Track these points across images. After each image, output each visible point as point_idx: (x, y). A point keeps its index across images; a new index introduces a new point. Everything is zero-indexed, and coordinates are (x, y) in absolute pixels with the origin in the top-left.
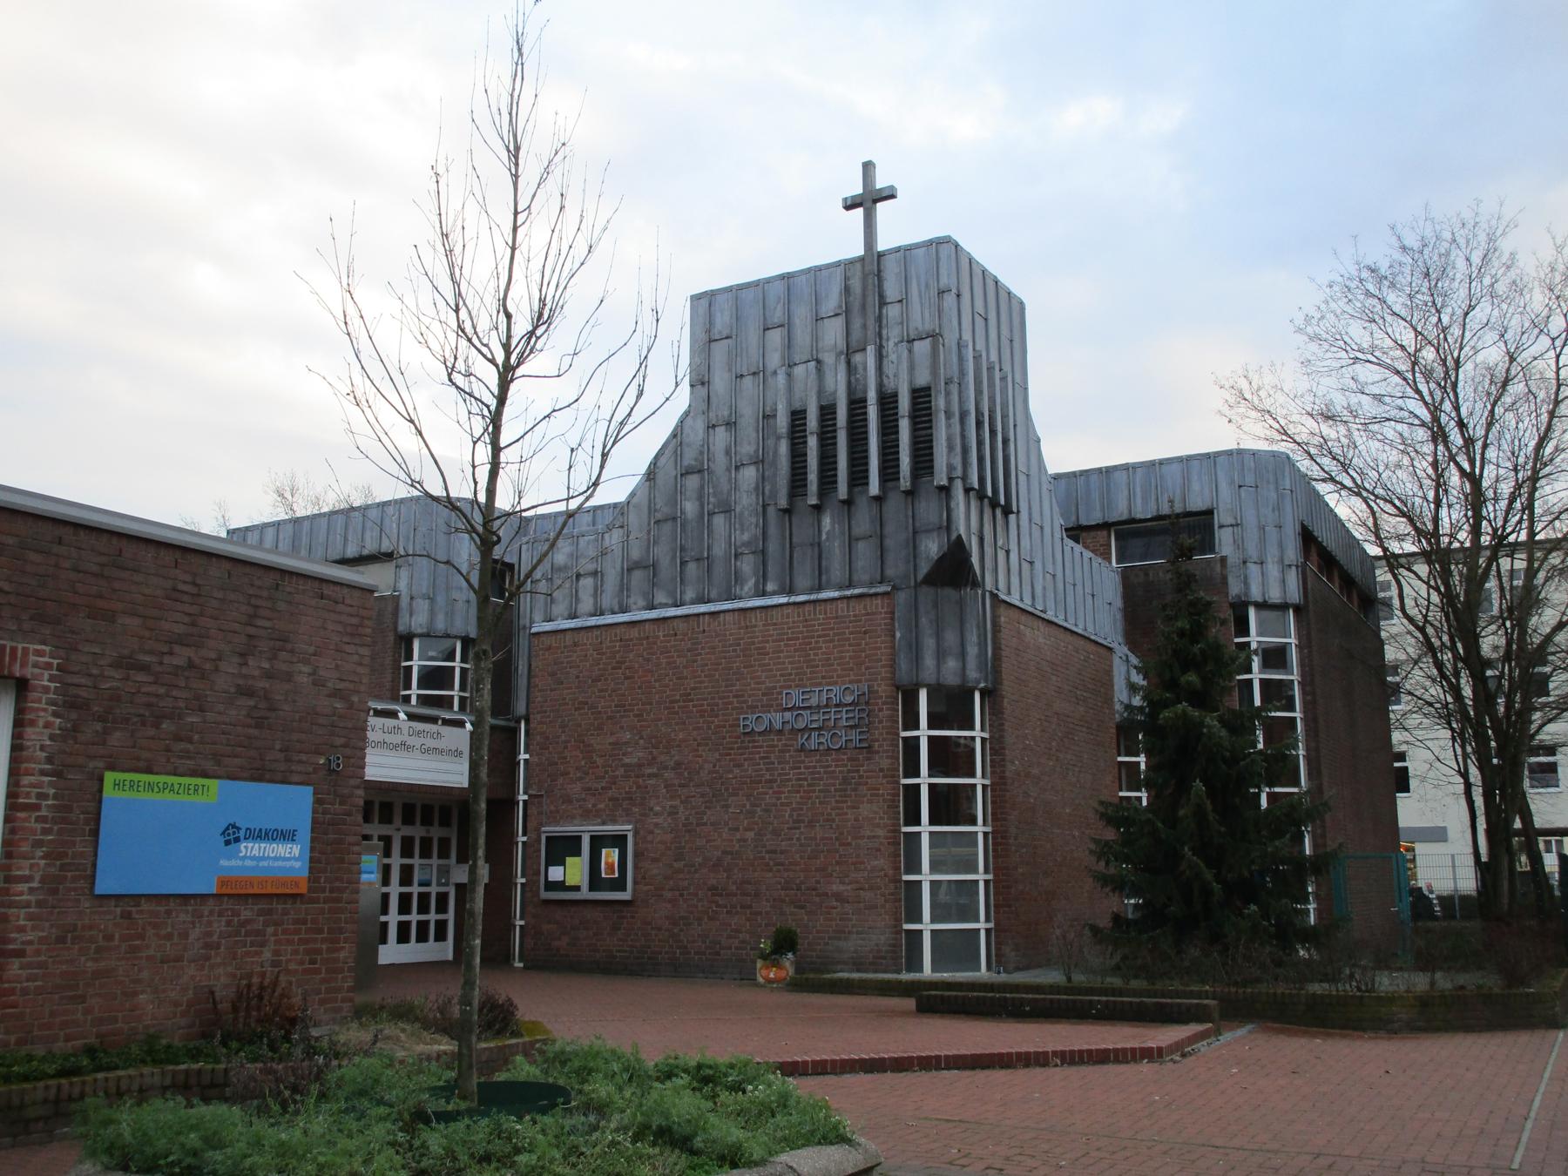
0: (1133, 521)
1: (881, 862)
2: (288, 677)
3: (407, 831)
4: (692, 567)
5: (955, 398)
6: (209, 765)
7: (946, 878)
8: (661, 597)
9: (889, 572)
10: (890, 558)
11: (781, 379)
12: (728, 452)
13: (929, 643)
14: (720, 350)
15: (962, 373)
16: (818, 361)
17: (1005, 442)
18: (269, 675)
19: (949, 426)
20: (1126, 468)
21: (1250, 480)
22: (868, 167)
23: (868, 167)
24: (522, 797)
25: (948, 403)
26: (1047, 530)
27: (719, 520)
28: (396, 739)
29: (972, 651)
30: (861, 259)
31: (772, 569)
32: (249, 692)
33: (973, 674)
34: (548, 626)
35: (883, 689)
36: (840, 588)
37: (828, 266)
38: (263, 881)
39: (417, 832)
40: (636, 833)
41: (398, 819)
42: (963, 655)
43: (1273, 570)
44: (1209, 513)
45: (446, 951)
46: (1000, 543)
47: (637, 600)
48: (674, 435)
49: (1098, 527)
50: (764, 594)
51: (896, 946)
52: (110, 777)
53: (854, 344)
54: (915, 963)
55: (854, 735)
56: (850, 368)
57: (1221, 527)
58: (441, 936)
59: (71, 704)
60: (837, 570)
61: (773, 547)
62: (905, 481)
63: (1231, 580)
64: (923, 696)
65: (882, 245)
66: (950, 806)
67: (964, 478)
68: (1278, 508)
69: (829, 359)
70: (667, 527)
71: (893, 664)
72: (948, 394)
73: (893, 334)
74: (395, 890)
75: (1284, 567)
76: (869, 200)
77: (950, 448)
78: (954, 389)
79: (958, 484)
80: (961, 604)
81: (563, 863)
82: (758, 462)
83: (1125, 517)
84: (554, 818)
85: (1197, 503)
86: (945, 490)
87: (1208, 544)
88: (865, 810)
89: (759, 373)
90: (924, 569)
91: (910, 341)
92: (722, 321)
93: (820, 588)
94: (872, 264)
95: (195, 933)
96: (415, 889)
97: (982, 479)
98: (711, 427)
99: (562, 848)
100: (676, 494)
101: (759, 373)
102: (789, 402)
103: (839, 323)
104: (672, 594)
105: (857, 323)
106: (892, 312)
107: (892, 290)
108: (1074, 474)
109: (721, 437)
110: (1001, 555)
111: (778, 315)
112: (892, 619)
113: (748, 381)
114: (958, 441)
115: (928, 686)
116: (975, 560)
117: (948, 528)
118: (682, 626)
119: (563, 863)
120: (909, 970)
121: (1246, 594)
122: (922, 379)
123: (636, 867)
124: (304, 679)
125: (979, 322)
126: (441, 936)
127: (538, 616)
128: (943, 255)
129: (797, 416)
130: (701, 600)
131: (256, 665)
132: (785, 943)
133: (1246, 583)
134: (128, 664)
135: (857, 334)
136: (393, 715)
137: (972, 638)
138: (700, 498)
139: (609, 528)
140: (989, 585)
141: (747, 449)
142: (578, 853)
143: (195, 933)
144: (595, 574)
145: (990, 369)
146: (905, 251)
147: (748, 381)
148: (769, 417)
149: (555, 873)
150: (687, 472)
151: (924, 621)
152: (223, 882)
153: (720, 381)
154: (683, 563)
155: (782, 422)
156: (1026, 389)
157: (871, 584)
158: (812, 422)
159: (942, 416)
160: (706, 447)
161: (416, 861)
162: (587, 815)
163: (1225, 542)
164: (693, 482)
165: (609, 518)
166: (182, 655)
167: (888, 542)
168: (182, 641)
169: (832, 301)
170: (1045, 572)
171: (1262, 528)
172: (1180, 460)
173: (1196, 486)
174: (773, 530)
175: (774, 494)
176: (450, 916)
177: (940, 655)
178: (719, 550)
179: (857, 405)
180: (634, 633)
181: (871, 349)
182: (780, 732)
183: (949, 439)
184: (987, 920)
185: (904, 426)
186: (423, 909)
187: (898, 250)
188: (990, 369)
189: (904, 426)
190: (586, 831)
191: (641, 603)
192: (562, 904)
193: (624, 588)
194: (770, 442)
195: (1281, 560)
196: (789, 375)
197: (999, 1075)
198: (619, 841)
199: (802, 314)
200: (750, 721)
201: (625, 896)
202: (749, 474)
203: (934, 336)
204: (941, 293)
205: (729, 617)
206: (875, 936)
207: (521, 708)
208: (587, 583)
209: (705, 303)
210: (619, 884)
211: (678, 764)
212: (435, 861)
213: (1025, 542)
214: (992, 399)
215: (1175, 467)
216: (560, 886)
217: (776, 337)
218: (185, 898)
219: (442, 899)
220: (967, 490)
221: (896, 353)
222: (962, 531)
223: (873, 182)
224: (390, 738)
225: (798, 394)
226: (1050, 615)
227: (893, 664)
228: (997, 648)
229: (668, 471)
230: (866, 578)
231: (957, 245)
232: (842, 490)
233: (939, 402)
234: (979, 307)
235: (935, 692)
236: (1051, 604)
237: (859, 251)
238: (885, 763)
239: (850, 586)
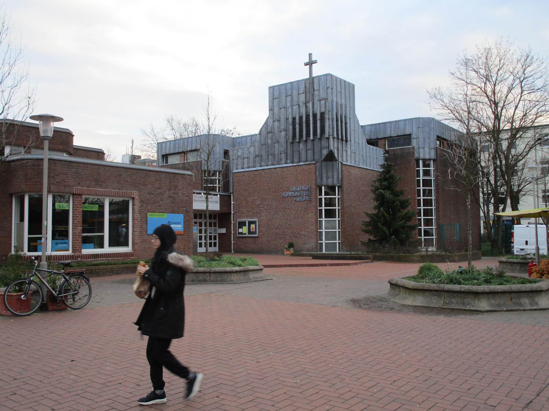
0: (391, 137)
1: (313, 227)
2: (178, 193)
4: (270, 156)
6: (165, 211)
7: (329, 229)
8: (263, 164)
9: (315, 158)
11: (290, 110)
13: (324, 175)
14: (276, 101)
15: (332, 109)
17: (346, 124)
18: (174, 193)
19: (329, 122)
20: (390, 122)
22: (310, 55)
23: (310, 55)
24: (232, 212)
26: (361, 143)
27: (276, 145)
29: (335, 177)
30: (308, 79)
31: (289, 157)
32: (170, 197)
33: (335, 182)
34: (237, 171)
35: (314, 186)
42: (333, 178)
43: (427, 150)
44: (410, 135)
46: (344, 149)
48: (265, 123)
49: (382, 138)
50: (287, 163)
51: (317, 246)
52: (148, 214)
53: (307, 101)
54: (321, 250)
55: (307, 197)
56: (306, 107)
58: (215, 246)
59: (141, 201)
60: (303, 157)
61: (289, 151)
62: (318, 136)
63: (415, 153)
64: (323, 188)
67: (333, 135)
68: (429, 133)
69: (301, 104)
70: (264, 146)
71: (316, 180)
72: (329, 114)
73: (316, 98)
74: (203, 235)
75: (430, 149)
76: (310, 63)
77: (329, 128)
78: (330, 113)
80: (333, 165)
81: (242, 228)
82: (285, 130)
84: (240, 217)
85: (407, 132)
86: (328, 138)
87: (410, 143)
88: (310, 215)
89: (285, 108)
90: (323, 157)
91: (320, 100)
92: (276, 94)
94: (311, 80)
97: (338, 134)
98: (274, 121)
99: (242, 224)
101: (285, 108)
104: (266, 163)
105: (308, 95)
106: (316, 93)
107: (316, 87)
108: (376, 124)
110: (344, 153)
111: (289, 93)
113: (282, 110)
115: (422, 159)
116: (336, 155)
117: (329, 148)
118: (268, 171)
120: (320, 251)
121: (419, 156)
122: (323, 110)
124: (180, 194)
125: (339, 94)
126: (215, 246)
127: (234, 168)
128: (328, 78)
129: (294, 119)
130: (272, 165)
131: (172, 192)
132: (291, 245)
133: (419, 154)
134: (150, 193)
136: (200, 193)
137: (335, 173)
138: (272, 139)
139: (251, 147)
140: (340, 160)
141: (283, 127)
142: (245, 226)
144: (248, 158)
146: (319, 77)
147: (282, 110)
148: (287, 119)
149: (240, 230)
151: (323, 170)
155: (290, 120)
156: (354, 108)
157: (311, 161)
158: (297, 121)
159: (327, 120)
160: (273, 127)
161: (208, 228)
162: (247, 216)
163: (414, 143)
164: (270, 135)
167: (315, 151)
169: (302, 90)
171: (424, 139)
172: (403, 120)
173: (407, 128)
174: (289, 147)
176: (209, 241)
177: (327, 178)
178: (276, 152)
179: (308, 116)
180: (257, 172)
181: (311, 102)
183: (329, 126)
184: (339, 240)
185: (318, 122)
186: (210, 239)
187: (317, 77)
188: (341, 105)
189: (318, 122)
190: (247, 220)
191: (259, 165)
192: (241, 237)
193: (254, 161)
194: (288, 125)
196: (292, 108)
198: (254, 223)
199: (295, 93)
200: (284, 194)
202: (283, 133)
203: (326, 99)
204: (327, 88)
205: (279, 169)
206: (311, 244)
207: (231, 191)
208: (246, 160)
209: (272, 89)
210: (254, 233)
211: (268, 204)
212: (213, 228)
213: (353, 148)
214: (342, 113)
215: (402, 122)
216: (242, 233)
217: (289, 98)
219: (215, 237)
220: (334, 138)
222: (332, 147)
223: (312, 59)
224: (200, 199)
225: (294, 113)
226: (361, 166)
227: (316, 180)
228: (342, 176)
229: (264, 132)
230: (310, 159)
231: (332, 75)
232: (304, 139)
233: (327, 116)
234: (339, 90)
237: (308, 77)
239: (306, 161)
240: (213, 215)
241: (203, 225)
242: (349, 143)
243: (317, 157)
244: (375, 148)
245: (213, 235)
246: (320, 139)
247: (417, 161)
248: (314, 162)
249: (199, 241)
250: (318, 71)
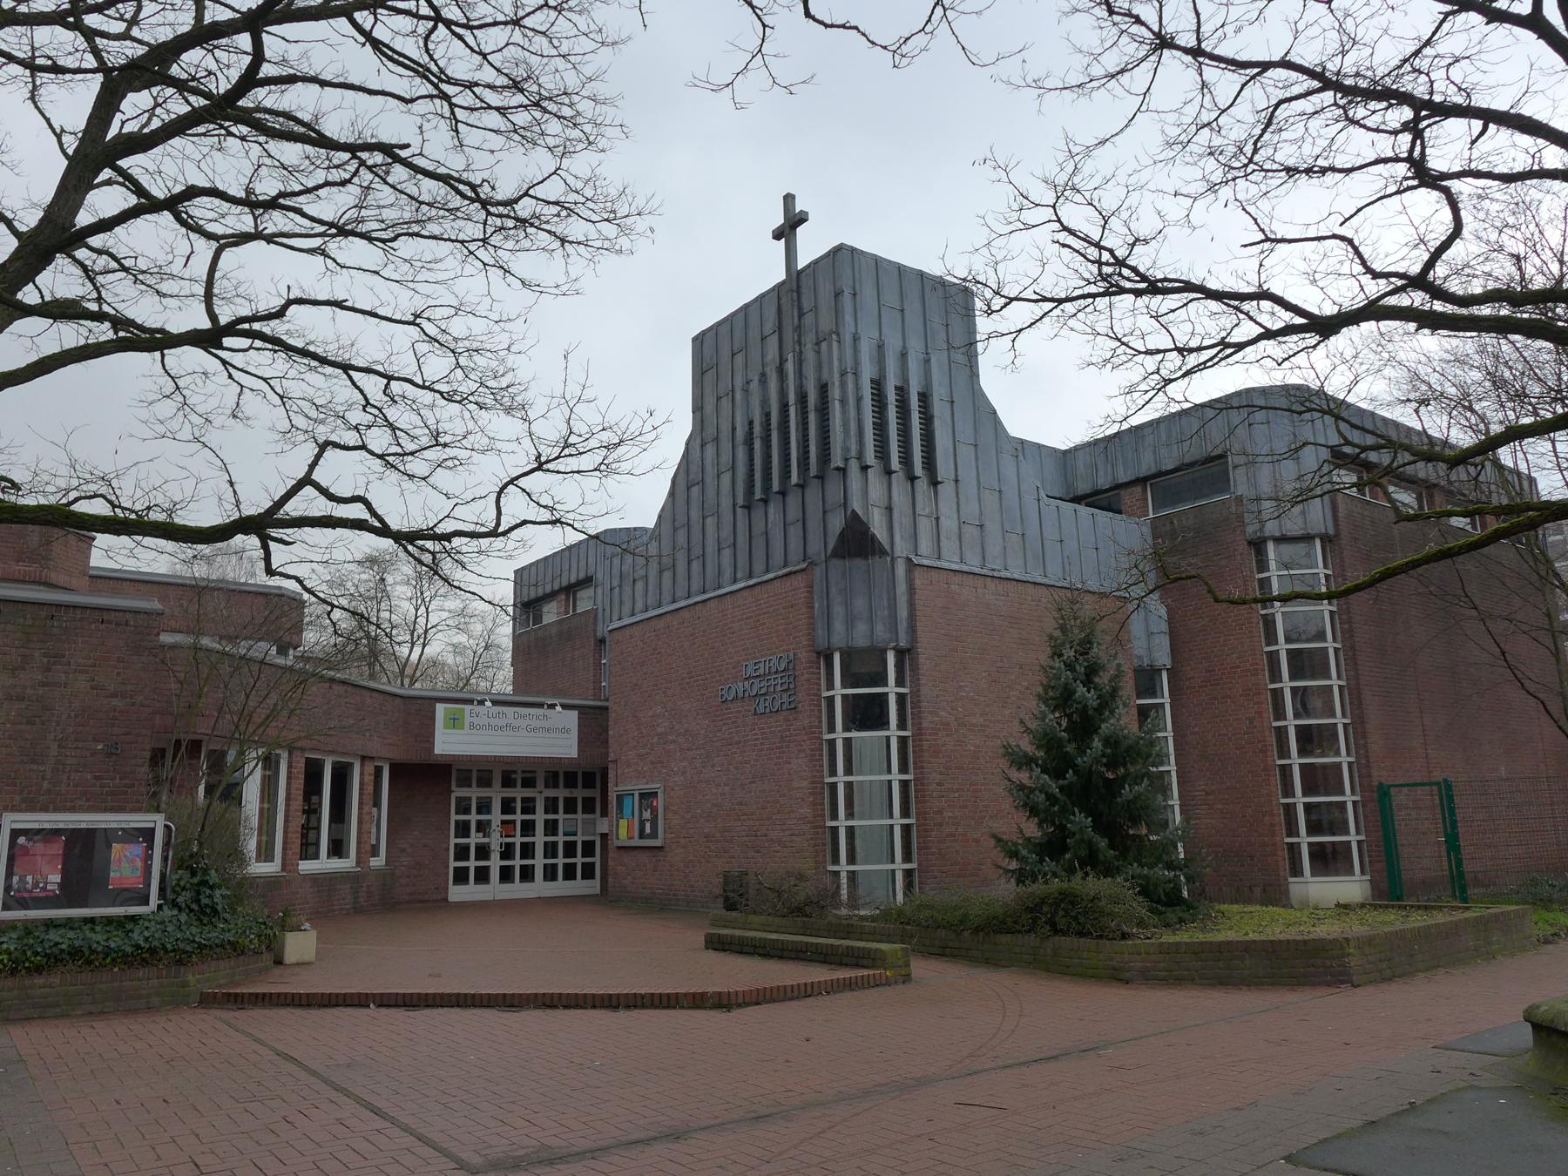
1: (806, 811)
3: (551, 793)
13: (838, 610)
22: (789, 199)
23: (789, 199)
28: (502, 722)
33: (881, 631)
35: (804, 655)
39: (561, 793)
41: (540, 784)
45: (593, 887)
57: (1235, 467)
58: (588, 872)
60: (778, 557)
63: (1248, 518)
67: (860, 457)
71: (812, 627)
76: (788, 229)
77: (846, 431)
78: (850, 378)
79: (854, 467)
83: (1153, 471)
86: (843, 471)
90: (831, 545)
96: (561, 839)
112: (811, 592)
117: (845, 504)
136: (552, 706)
140: (901, 548)
163: (1240, 484)
176: (597, 860)
177: (850, 621)
180: (661, 624)
183: (845, 424)
189: (812, 417)
197: (455, 1013)
210: (654, 835)
212: (580, 816)
213: (971, 509)
222: (856, 505)
224: (493, 722)
231: (853, 250)
235: (848, 655)
240: (556, 774)
241: (540, 807)
242: (946, 490)
243: (815, 546)
244: (1103, 516)
245: (579, 839)
246: (821, 477)
247: (1258, 545)
248: (804, 565)
250: (811, 245)
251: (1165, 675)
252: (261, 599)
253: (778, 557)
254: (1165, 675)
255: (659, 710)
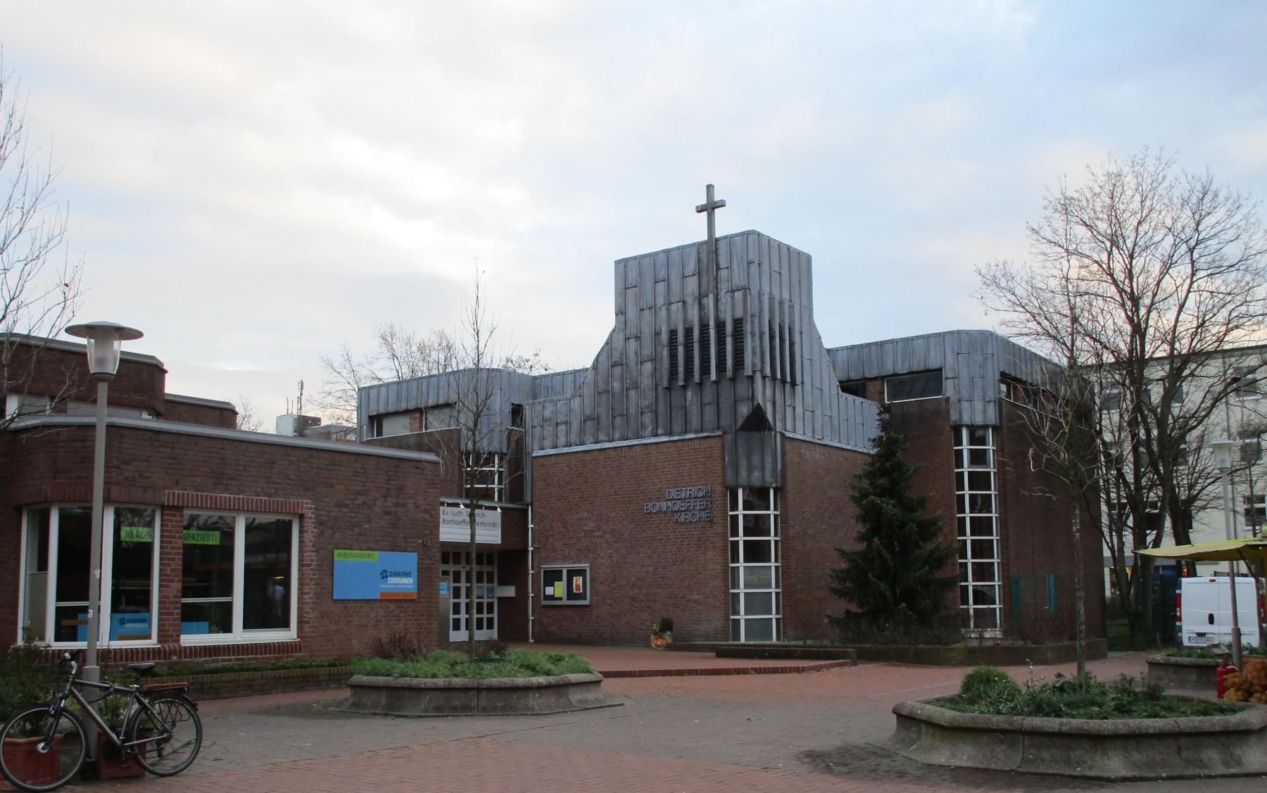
1: (718, 583)
2: (404, 505)
4: (618, 419)
5: (757, 324)
7: (755, 588)
8: (602, 437)
9: (723, 423)
10: (723, 415)
11: (664, 312)
12: (636, 353)
13: (743, 462)
15: (761, 310)
16: (684, 302)
17: (792, 344)
18: (397, 505)
19: (753, 341)
20: (892, 341)
21: (964, 349)
22: (710, 188)
23: (710, 188)
24: (531, 549)
25: (753, 327)
27: (632, 393)
29: (768, 466)
30: (706, 242)
31: (661, 422)
33: (769, 479)
34: (542, 453)
35: (718, 489)
36: (697, 432)
37: (689, 246)
38: (398, 594)
40: (591, 568)
42: (763, 469)
43: (978, 405)
44: (940, 370)
46: (788, 403)
47: (589, 438)
48: (607, 343)
50: (656, 435)
52: (336, 552)
55: (703, 514)
56: (701, 306)
58: (490, 626)
59: (320, 523)
60: (695, 423)
61: (661, 409)
62: (729, 373)
64: (740, 492)
65: (718, 234)
66: (756, 552)
67: (762, 370)
68: (983, 366)
69: (689, 300)
70: (604, 397)
72: (752, 322)
73: (724, 287)
74: (463, 600)
75: (986, 402)
76: (710, 208)
77: (754, 353)
79: (758, 377)
80: (762, 440)
81: (553, 585)
82: (653, 359)
84: (547, 561)
85: (933, 364)
88: (709, 554)
89: (653, 308)
90: (740, 422)
91: (733, 291)
92: (632, 276)
93: (686, 432)
94: (712, 246)
95: (372, 615)
99: (552, 577)
100: (610, 376)
101: (653, 308)
102: (668, 326)
103: (694, 280)
105: (704, 280)
106: (724, 274)
108: (861, 346)
109: (632, 344)
110: (789, 411)
111: (662, 274)
113: (646, 312)
114: (758, 350)
116: (769, 416)
118: (613, 453)
119: (553, 585)
122: (739, 314)
123: (591, 587)
126: (490, 626)
127: (536, 447)
129: (673, 333)
131: (390, 502)
132: (666, 626)
133: (960, 414)
134: (340, 505)
135: (704, 288)
136: (457, 505)
137: (769, 459)
139: (573, 397)
140: (779, 427)
141: (647, 352)
143: (372, 615)
144: (566, 423)
145: (781, 303)
146: (730, 238)
148: (657, 334)
150: (614, 365)
151: (740, 451)
152: (382, 594)
153: (632, 312)
154: (613, 417)
155: (665, 337)
157: (712, 431)
160: (625, 353)
161: (475, 585)
162: (565, 559)
163: (949, 389)
164: (618, 370)
165: (621, 337)
166: (361, 499)
167: (721, 406)
168: (360, 493)
169: (691, 267)
170: (823, 415)
172: (923, 337)
173: (933, 353)
174: (661, 400)
175: (661, 380)
177: (750, 470)
178: (632, 410)
179: (704, 327)
180: (588, 457)
181: (711, 296)
182: (665, 513)
183: (753, 349)
184: (777, 613)
185: (729, 341)
186: (480, 611)
187: (726, 237)
188: (781, 303)
189: (729, 341)
190: (565, 567)
192: (550, 607)
193: (582, 431)
194: (659, 348)
195: (984, 399)
196: (668, 310)
198: (581, 572)
201: (587, 602)
202: (648, 367)
203: (745, 289)
204: (749, 263)
207: (528, 499)
208: (562, 428)
209: (623, 266)
210: (583, 596)
211: (613, 530)
212: (485, 585)
213: (808, 400)
214: (782, 320)
216: (552, 597)
217: (661, 287)
218: (368, 601)
219: (490, 606)
220: (764, 377)
221: (725, 298)
222: (760, 400)
224: (456, 518)
226: (826, 441)
229: (604, 363)
230: (710, 426)
231: (759, 234)
232: (697, 378)
234: (775, 266)
236: (828, 432)
237: (705, 237)
238: (720, 529)
239: (702, 431)
240: (485, 554)
242: (798, 389)
245: (485, 600)
247: (957, 429)
249: (452, 616)
250: (727, 224)
251: (772, 492)
252: (217, 413)
253: (695, 423)
254: (772, 492)
255: (586, 514)
